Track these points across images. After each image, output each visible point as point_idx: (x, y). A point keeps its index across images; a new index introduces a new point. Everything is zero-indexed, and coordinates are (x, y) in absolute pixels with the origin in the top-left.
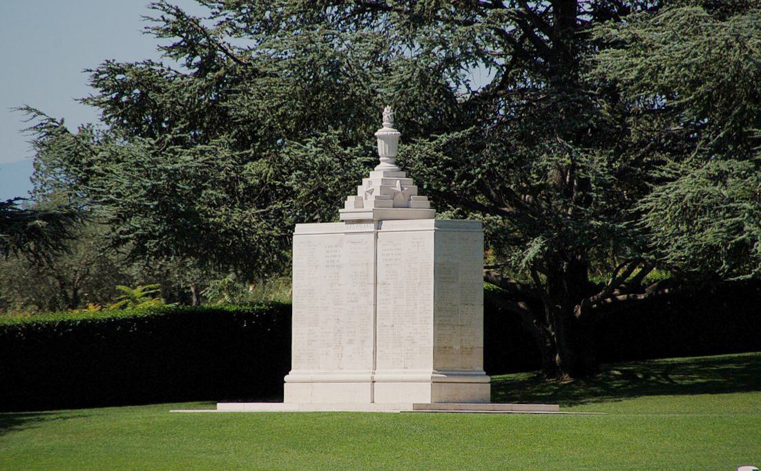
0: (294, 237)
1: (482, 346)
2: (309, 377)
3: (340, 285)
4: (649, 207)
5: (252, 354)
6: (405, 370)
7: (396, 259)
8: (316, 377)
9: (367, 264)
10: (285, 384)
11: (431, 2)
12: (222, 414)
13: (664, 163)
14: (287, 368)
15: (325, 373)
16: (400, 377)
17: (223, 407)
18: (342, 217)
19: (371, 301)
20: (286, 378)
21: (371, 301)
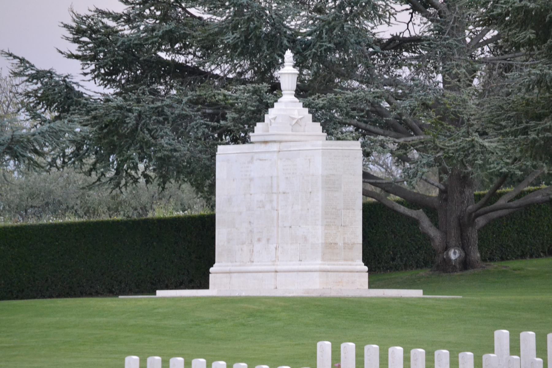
0: (217, 156)
1: (361, 242)
2: (227, 269)
3: (251, 194)
4: (400, 150)
5: (185, 250)
6: (300, 262)
7: (293, 173)
8: (233, 269)
9: (272, 177)
10: (210, 275)
11: (488, 2)
12: (164, 298)
13: (167, 143)
14: (211, 262)
15: (240, 266)
16: (296, 267)
17: (160, 293)
18: (252, 139)
19: (288, 200)
20: (211, 270)
21: (288, 200)
